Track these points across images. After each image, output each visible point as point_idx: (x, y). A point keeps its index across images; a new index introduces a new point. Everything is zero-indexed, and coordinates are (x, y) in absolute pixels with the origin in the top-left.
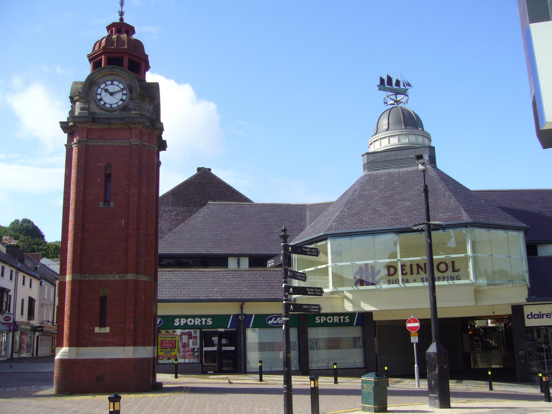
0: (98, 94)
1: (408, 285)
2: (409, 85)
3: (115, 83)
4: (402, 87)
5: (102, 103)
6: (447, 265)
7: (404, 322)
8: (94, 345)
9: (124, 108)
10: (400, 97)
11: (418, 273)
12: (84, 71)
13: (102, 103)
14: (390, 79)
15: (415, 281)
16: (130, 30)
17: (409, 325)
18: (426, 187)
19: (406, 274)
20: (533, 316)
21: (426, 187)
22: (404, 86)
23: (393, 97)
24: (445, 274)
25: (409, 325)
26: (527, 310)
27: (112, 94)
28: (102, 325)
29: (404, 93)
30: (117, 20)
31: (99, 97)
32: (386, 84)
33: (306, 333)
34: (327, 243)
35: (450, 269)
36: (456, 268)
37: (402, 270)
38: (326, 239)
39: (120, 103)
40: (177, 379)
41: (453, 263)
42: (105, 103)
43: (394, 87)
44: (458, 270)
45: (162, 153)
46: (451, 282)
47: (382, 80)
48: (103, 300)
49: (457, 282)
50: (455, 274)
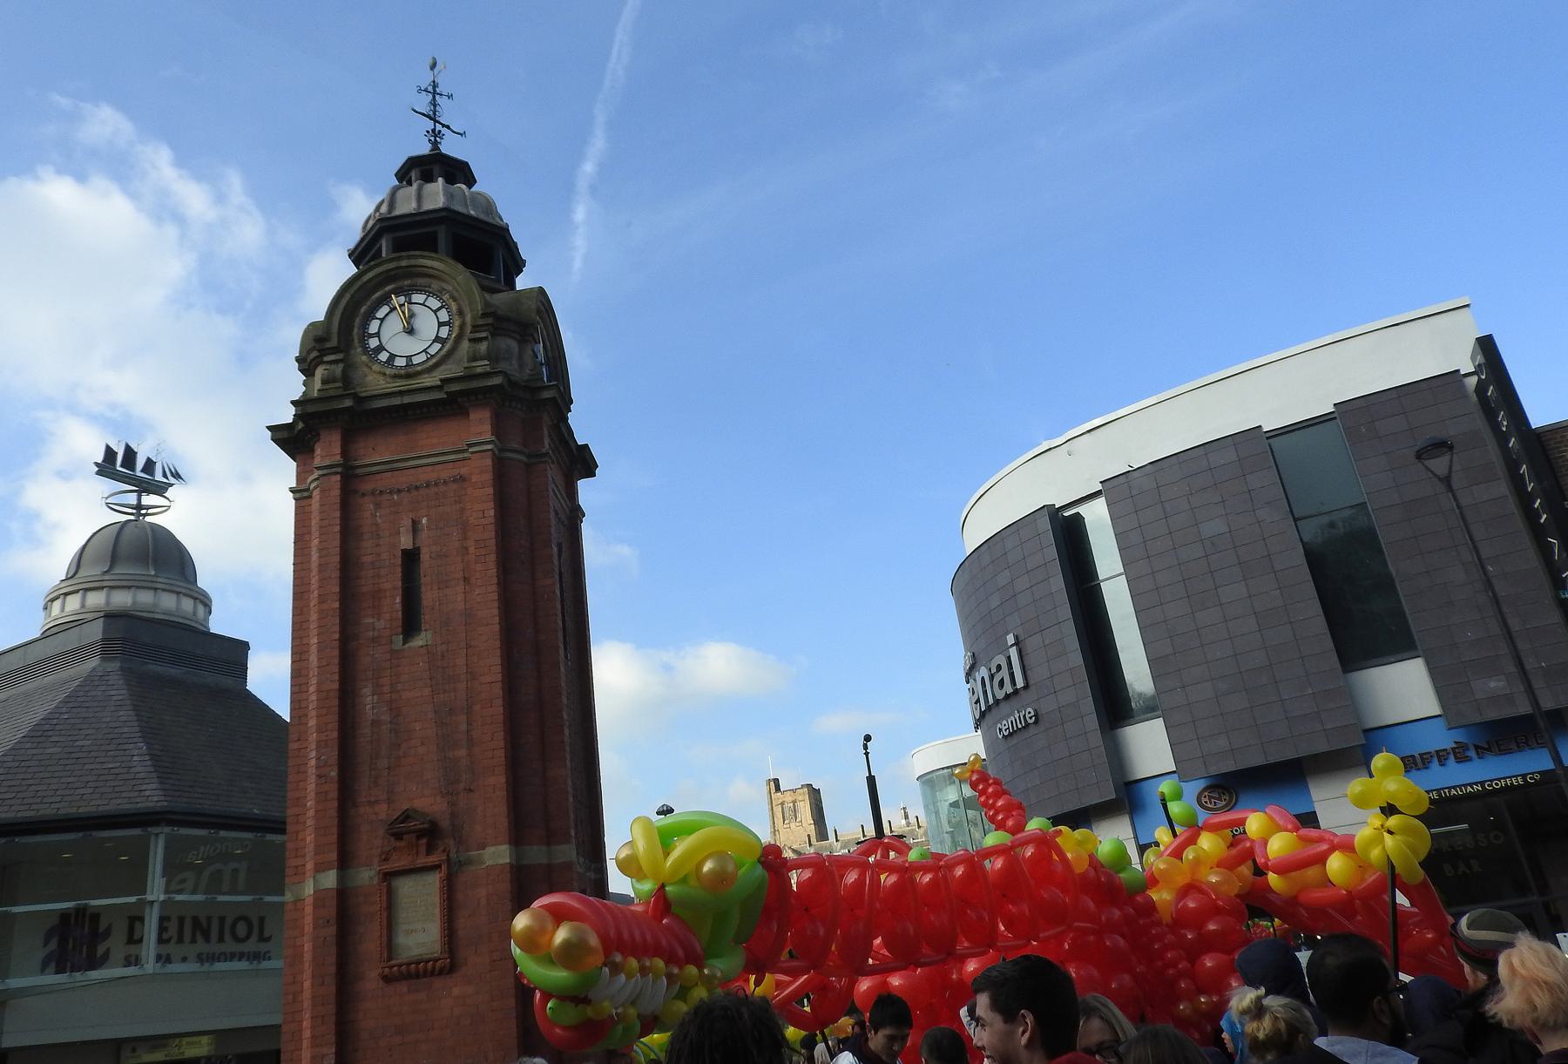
0: (371, 336)
1: (171, 968)
2: (177, 476)
4: (159, 477)
5: (383, 356)
10: (148, 500)
11: (193, 941)
12: (328, 274)
13: (383, 356)
14: (130, 455)
15: (184, 960)
16: (458, 172)
19: (168, 941)
22: (165, 476)
23: (132, 499)
29: (160, 489)
30: (424, 149)
31: (373, 343)
32: (120, 466)
36: (266, 934)
37: (162, 929)
38: (156, 823)
41: (262, 920)
42: (392, 357)
43: (139, 474)
44: (268, 939)
45: (583, 485)
46: (255, 965)
47: (110, 454)
50: (263, 947)
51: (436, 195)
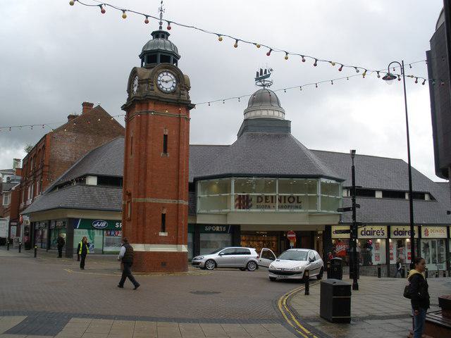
3: (169, 74)
6: (262, 198)
7: (287, 233)
8: (159, 243)
9: (173, 92)
17: (289, 236)
18: (353, 167)
20: (337, 232)
21: (353, 167)
24: (262, 204)
25: (289, 236)
26: (334, 229)
27: (167, 82)
28: (164, 231)
30: (158, 29)
33: (199, 237)
34: (231, 180)
35: (296, 201)
39: (172, 88)
40: (82, 272)
48: (164, 216)
49: (266, 210)
50: (298, 205)
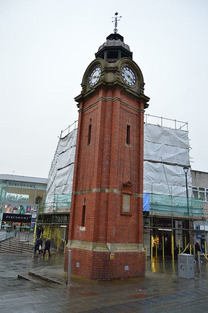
30: (113, 33)
51: (117, 43)
